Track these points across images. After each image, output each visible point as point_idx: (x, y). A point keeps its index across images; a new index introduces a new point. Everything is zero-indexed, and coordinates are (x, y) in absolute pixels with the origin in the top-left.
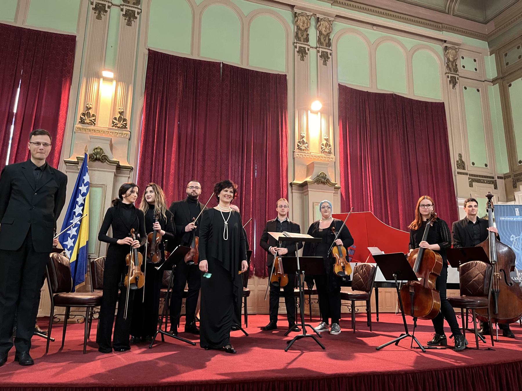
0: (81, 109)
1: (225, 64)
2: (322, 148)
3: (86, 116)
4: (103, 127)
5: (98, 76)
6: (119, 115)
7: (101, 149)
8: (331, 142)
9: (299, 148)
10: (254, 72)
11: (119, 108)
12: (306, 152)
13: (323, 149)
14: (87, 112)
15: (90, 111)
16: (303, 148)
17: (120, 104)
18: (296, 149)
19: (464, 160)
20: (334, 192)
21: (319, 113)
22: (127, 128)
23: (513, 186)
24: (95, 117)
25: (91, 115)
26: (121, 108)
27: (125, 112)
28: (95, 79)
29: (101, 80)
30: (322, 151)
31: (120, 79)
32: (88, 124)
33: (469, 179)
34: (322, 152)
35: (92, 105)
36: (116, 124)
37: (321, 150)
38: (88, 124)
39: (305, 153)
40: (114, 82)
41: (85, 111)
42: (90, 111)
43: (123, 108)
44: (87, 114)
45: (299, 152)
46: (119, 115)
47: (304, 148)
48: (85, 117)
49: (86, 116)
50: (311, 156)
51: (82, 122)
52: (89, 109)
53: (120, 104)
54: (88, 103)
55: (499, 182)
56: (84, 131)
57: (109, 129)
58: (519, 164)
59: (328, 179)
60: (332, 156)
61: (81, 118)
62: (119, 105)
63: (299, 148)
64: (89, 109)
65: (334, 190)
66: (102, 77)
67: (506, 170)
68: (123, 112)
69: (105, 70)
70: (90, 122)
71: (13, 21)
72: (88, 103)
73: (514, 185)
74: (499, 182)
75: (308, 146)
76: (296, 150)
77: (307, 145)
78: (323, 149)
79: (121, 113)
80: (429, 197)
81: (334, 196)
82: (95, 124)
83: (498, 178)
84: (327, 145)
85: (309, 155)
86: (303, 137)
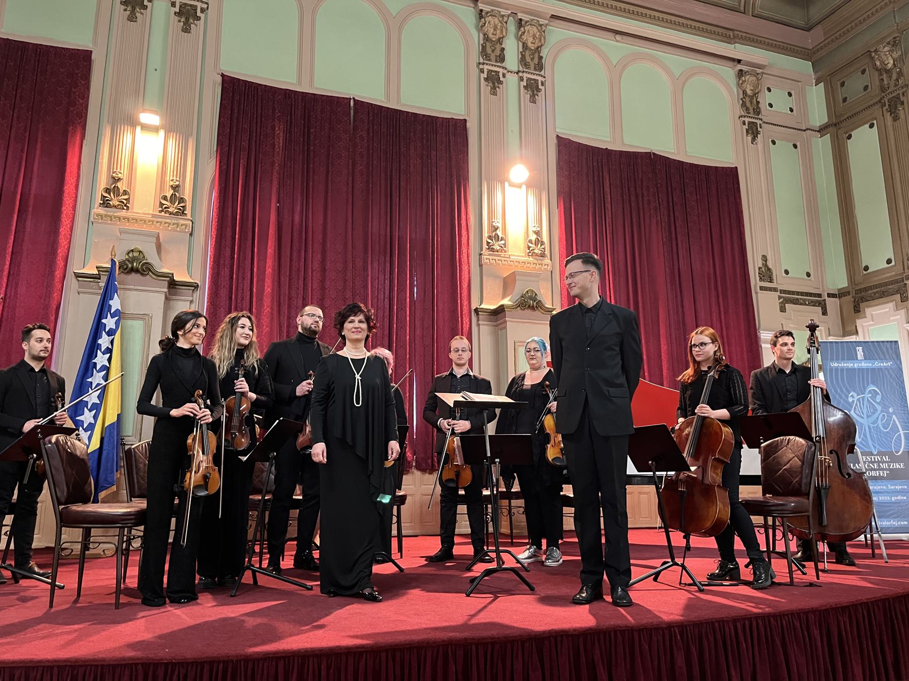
0: (103, 182)
2: (529, 248)
5: (133, 123)
6: (172, 192)
8: (545, 237)
9: (490, 248)
12: (503, 254)
13: (531, 249)
15: (119, 184)
16: (496, 247)
18: (484, 249)
19: (770, 267)
21: (524, 187)
22: (186, 214)
23: (854, 310)
25: (121, 191)
26: (175, 178)
27: (181, 186)
29: (138, 128)
31: (170, 127)
33: (780, 298)
34: (530, 254)
35: (123, 173)
36: (166, 208)
37: (528, 251)
38: (115, 207)
40: (162, 133)
41: (110, 185)
42: (119, 184)
43: (178, 179)
45: (490, 255)
46: (172, 192)
47: (499, 248)
48: (110, 195)
49: (112, 194)
52: (496, 229)
54: (115, 170)
55: (832, 304)
57: (154, 216)
58: (865, 272)
60: (547, 261)
61: (103, 197)
62: (172, 173)
64: (496, 229)
67: (842, 282)
68: (178, 186)
69: (144, 111)
70: (118, 205)
73: (855, 307)
74: (832, 304)
75: (505, 244)
77: (503, 242)
78: (531, 249)
79: (175, 188)
83: (829, 295)
84: (539, 242)
85: (506, 259)
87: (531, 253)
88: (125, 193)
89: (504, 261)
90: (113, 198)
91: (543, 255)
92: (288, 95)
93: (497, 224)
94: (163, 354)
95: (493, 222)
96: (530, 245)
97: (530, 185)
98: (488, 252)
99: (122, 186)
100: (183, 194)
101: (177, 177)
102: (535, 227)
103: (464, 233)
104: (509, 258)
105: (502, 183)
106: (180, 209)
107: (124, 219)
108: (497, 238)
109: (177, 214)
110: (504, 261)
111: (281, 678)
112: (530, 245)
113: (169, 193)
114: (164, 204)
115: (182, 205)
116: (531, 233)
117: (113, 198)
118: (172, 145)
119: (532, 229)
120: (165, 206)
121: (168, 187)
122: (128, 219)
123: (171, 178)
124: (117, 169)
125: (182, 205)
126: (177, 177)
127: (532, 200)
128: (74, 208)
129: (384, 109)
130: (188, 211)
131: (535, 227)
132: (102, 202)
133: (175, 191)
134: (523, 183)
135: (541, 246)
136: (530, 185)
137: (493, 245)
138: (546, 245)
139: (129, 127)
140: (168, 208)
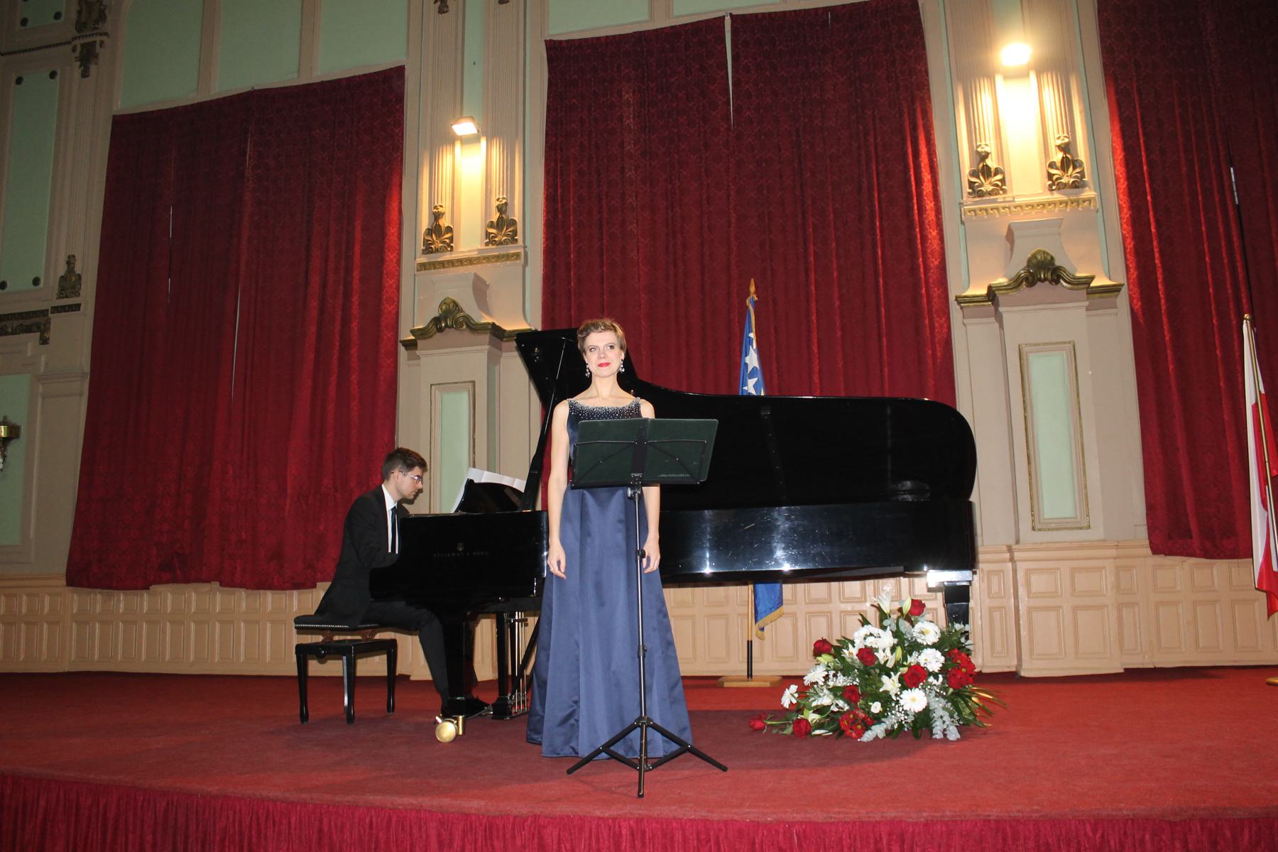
0: (425, 222)
1: (738, 16)
2: (1050, 176)
3: (434, 236)
4: (469, 251)
5: (451, 140)
6: (1060, 155)
7: (1044, 252)
8: (1082, 153)
9: (976, 192)
10: (760, 16)
11: (497, 198)
12: (1000, 198)
13: (1055, 178)
14: (981, 165)
15: (989, 162)
16: (987, 187)
17: (499, 189)
18: (965, 195)
20: (1086, 303)
21: (1033, 75)
22: (517, 240)
24: (1003, 173)
25: (993, 170)
26: (501, 197)
27: (509, 205)
28: (986, 80)
29: (999, 79)
30: (1053, 184)
31: (490, 131)
32: (990, 193)
34: (1054, 187)
35: (988, 145)
36: (1057, 179)
38: (990, 193)
39: (995, 201)
40: (483, 141)
41: (976, 165)
42: (989, 162)
43: (505, 196)
44: (435, 230)
45: (976, 203)
46: (1060, 155)
47: (991, 188)
48: (432, 238)
49: (981, 177)
50: (1015, 207)
51: (428, 250)
52: (985, 156)
53: (499, 189)
54: (978, 143)
56: (985, 214)
57: (480, 251)
59: (1059, 268)
60: (1089, 193)
61: (971, 184)
62: (498, 191)
63: (976, 192)
64: (985, 156)
65: (1088, 299)
66: (457, 140)
68: (1067, 145)
69: (456, 122)
70: (993, 190)
71: (296, 75)
72: (978, 143)
75: (1003, 181)
76: (965, 199)
77: (999, 177)
78: (1055, 178)
79: (1065, 148)
80: (620, 332)
81: (1087, 316)
82: (452, 247)
84: (1069, 162)
85: (1007, 205)
86: (987, 155)
87: (1054, 184)
88: (997, 171)
89: (1004, 208)
90: (435, 239)
91: (1078, 185)
92: (640, 38)
93: (987, 149)
94: (652, 420)
95: (977, 147)
96: (1053, 171)
97: (1041, 68)
98: (971, 200)
99: (992, 163)
100: (1077, 155)
101: (503, 194)
102: (1059, 138)
103: (926, 176)
104: (1013, 201)
105: (990, 77)
106: (997, 185)
107: (1027, 206)
108: (987, 172)
109: (505, 242)
110: (1004, 208)
111: (148, 848)
112: (1053, 171)
113: (1058, 157)
114: (1054, 175)
115: (1078, 170)
116: (1053, 149)
117: (435, 239)
118: (496, 152)
119: (1054, 142)
120: (977, 184)
121: (1053, 149)
122: (1033, 206)
123: (497, 196)
124: (981, 142)
125: (1078, 170)
126: (1064, 133)
127: (1051, 96)
128: (938, 211)
129: (760, 16)
130: (519, 237)
131: (1059, 138)
132: (970, 191)
133: (1065, 153)
134: (1029, 68)
135: (507, 229)
136: (1041, 68)
137: (981, 185)
138: (1085, 165)
139: (986, 80)
140: (1061, 179)
